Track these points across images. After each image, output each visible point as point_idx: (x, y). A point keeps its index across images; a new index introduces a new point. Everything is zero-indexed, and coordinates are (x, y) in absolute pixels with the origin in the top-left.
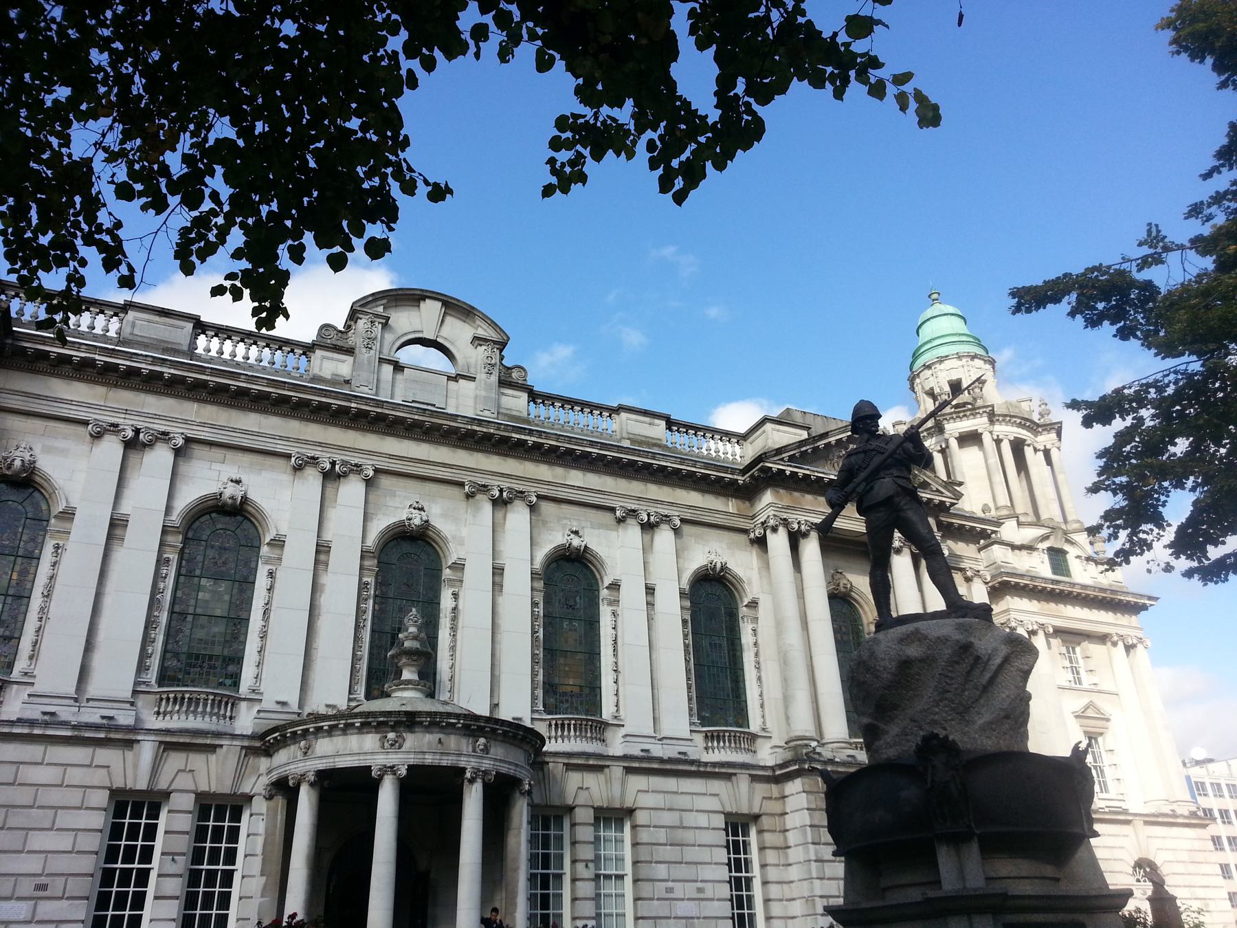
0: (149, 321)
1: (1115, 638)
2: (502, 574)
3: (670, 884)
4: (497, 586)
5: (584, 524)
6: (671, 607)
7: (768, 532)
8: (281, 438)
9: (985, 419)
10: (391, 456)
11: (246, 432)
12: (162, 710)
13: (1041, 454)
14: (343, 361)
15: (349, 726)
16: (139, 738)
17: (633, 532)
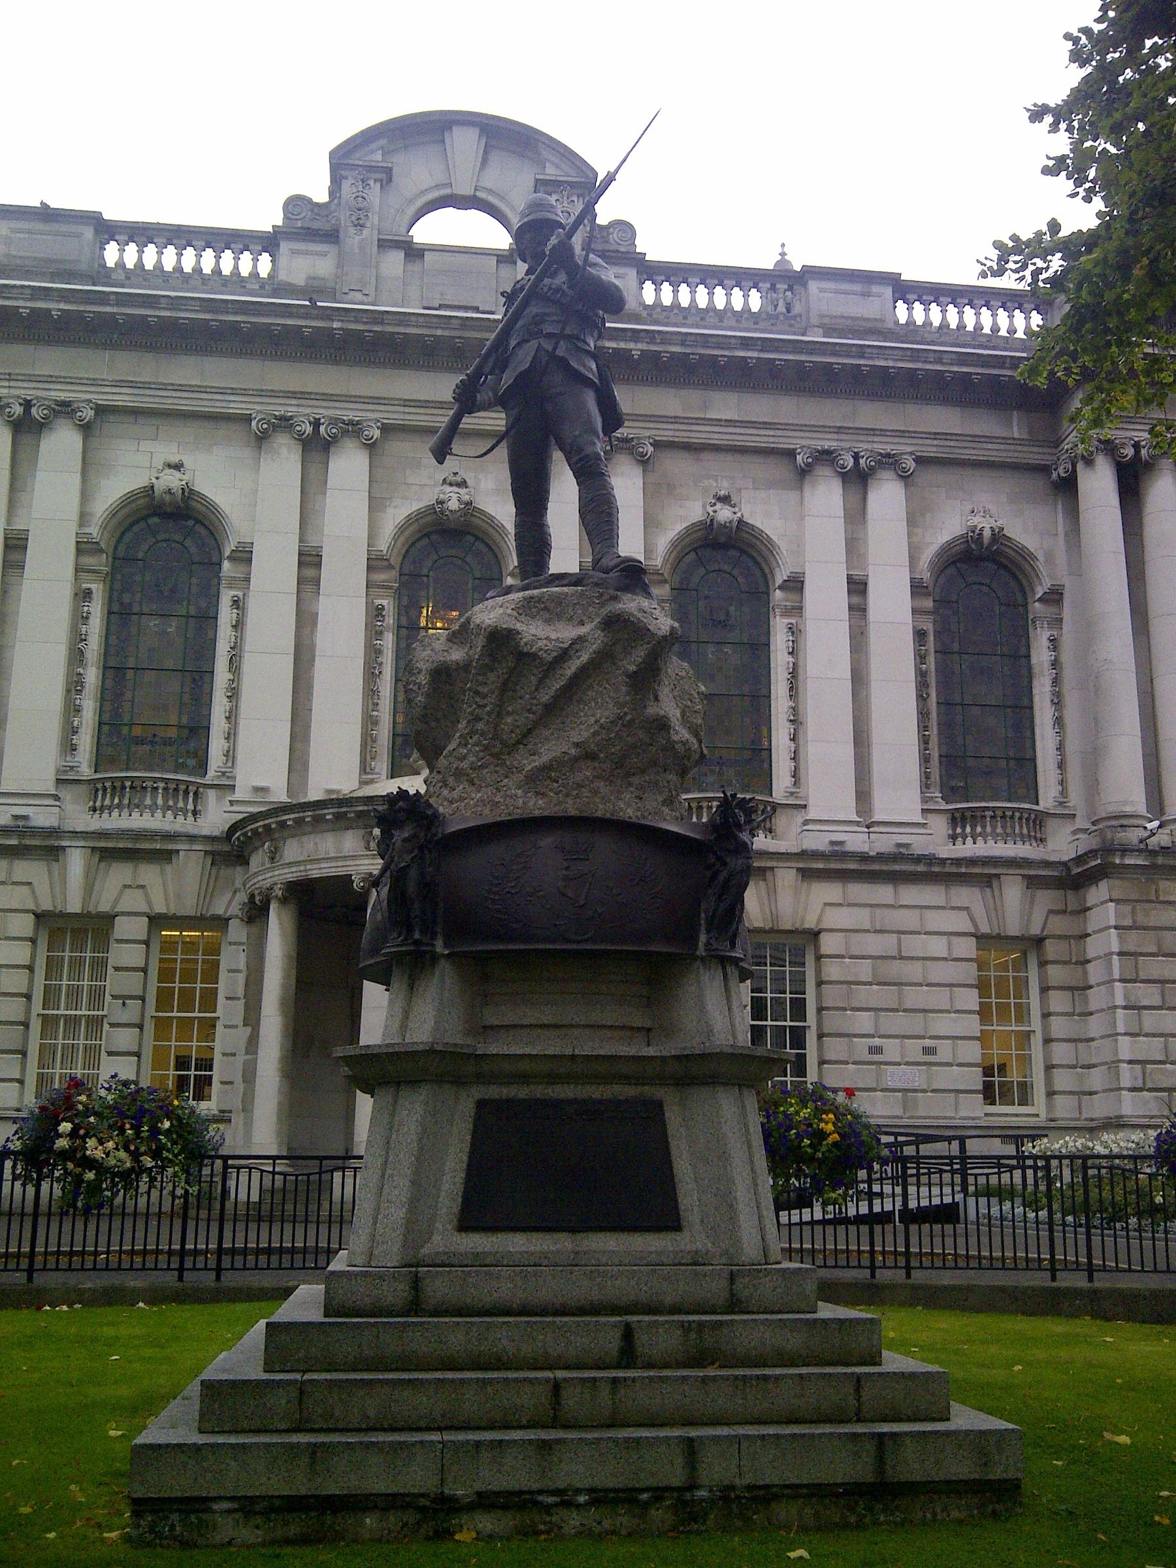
0: (30, 232)
2: (319, 565)
3: (877, 1041)
6: (893, 607)
7: (1080, 466)
8: (234, 392)
10: (406, 403)
11: (180, 388)
12: (98, 804)
14: (325, 254)
15: (318, 820)
16: (64, 843)
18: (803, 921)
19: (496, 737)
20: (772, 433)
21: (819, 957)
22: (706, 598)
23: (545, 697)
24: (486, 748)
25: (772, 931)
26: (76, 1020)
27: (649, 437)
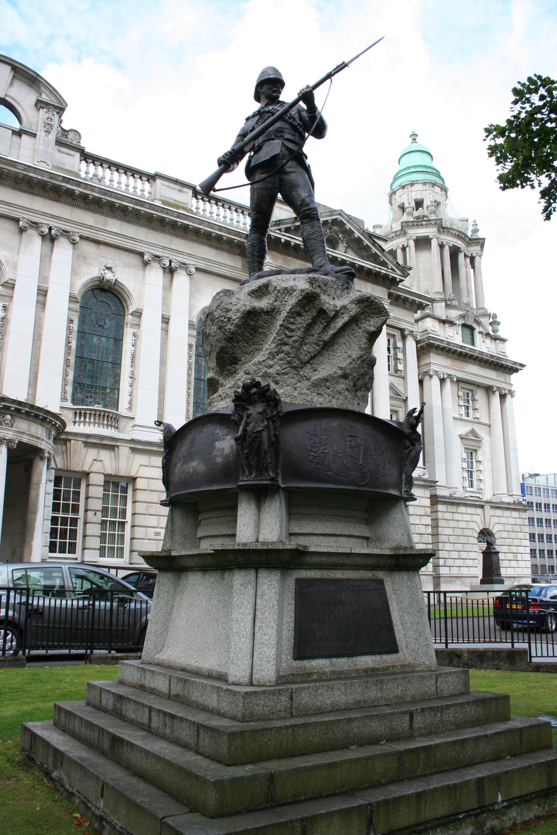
1: (495, 389)
4: (41, 304)
9: (435, 229)
13: (468, 260)
17: (155, 275)
18: (130, 472)
19: (297, 356)
21: (135, 490)
22: (96, 313)
24: (289, 362)
25: (115, 476)
26: (114, 522)
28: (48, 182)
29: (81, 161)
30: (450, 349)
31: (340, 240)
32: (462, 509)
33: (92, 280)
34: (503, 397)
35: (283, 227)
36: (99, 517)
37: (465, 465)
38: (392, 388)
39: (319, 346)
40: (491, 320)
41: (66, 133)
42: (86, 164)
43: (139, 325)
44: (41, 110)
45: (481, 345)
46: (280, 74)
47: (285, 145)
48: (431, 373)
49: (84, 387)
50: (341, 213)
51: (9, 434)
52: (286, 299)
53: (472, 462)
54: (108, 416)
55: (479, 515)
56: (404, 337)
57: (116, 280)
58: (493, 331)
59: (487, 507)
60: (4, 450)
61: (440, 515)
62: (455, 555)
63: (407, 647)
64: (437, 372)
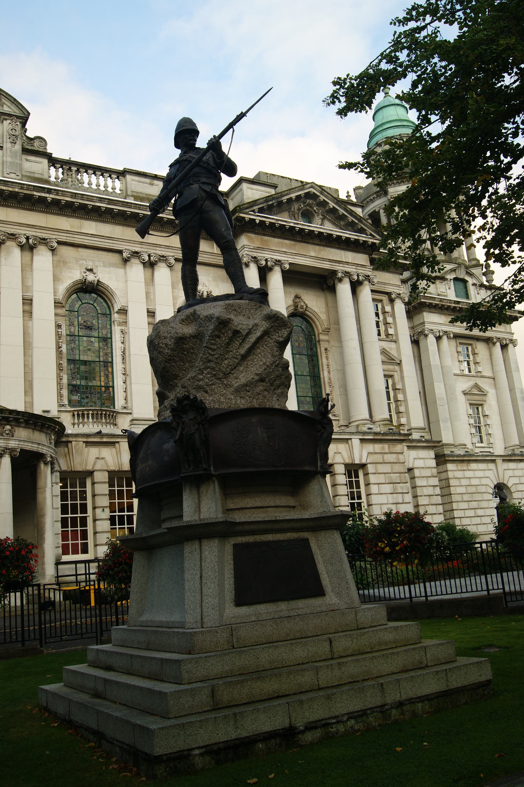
1: (495, 340)
2: (31, 304)
5: (97, 264)
17: (136, 270)
20: (112, 242)
23: (242, 351)
27: (55, 239)
28: (19, 193)
29: (49, 167)
30: (443, 305)
31: (316, 213)
32: (473, 466)
33: (75, 283)
34: (504, 347)
35: (256, 208)
36: (107, 514)
37: (472, 421)
38: (384, 352)
39: (237, 359)
40: (484, 270)
41: (32, 142)
42: (55, 169)
43: (126, 322)
44: (5, 122)
45: (475, 297)
46: (194, 124)
47: (202, 189)
48: (426, 332)
49: (79, 388)
50: (313, 185)
51: (12, 444)
52: (207, 325)
53: (479, 418)
54: (105, 414)
55: (492, 470)
56: (392, 301)
57: (98, 281)
58: (487, 281)
59: (499, 461)
60: (6, 460)
61: (450, 475)
62: (471, 513)
63: (332, 591)
64: (432, 330)
